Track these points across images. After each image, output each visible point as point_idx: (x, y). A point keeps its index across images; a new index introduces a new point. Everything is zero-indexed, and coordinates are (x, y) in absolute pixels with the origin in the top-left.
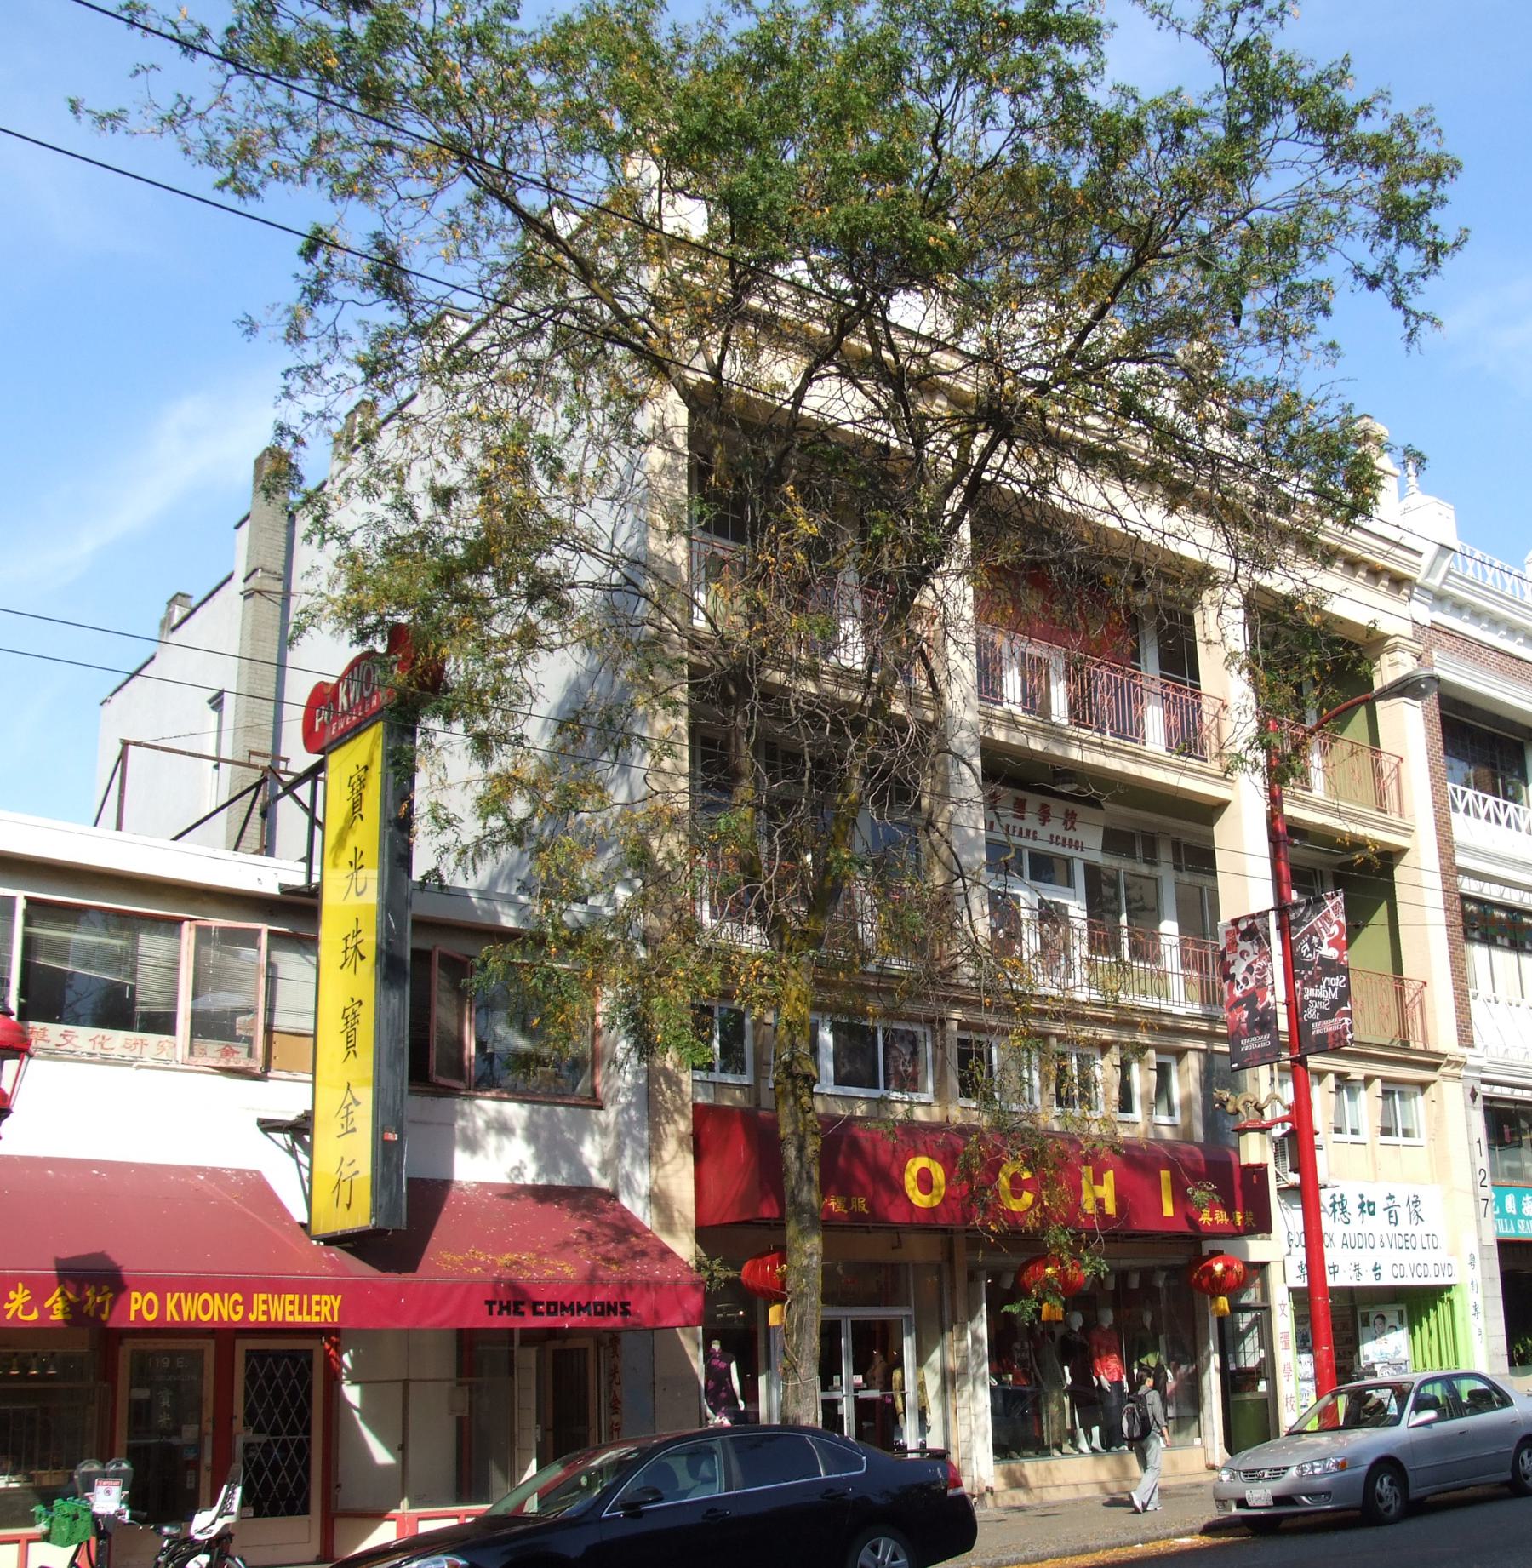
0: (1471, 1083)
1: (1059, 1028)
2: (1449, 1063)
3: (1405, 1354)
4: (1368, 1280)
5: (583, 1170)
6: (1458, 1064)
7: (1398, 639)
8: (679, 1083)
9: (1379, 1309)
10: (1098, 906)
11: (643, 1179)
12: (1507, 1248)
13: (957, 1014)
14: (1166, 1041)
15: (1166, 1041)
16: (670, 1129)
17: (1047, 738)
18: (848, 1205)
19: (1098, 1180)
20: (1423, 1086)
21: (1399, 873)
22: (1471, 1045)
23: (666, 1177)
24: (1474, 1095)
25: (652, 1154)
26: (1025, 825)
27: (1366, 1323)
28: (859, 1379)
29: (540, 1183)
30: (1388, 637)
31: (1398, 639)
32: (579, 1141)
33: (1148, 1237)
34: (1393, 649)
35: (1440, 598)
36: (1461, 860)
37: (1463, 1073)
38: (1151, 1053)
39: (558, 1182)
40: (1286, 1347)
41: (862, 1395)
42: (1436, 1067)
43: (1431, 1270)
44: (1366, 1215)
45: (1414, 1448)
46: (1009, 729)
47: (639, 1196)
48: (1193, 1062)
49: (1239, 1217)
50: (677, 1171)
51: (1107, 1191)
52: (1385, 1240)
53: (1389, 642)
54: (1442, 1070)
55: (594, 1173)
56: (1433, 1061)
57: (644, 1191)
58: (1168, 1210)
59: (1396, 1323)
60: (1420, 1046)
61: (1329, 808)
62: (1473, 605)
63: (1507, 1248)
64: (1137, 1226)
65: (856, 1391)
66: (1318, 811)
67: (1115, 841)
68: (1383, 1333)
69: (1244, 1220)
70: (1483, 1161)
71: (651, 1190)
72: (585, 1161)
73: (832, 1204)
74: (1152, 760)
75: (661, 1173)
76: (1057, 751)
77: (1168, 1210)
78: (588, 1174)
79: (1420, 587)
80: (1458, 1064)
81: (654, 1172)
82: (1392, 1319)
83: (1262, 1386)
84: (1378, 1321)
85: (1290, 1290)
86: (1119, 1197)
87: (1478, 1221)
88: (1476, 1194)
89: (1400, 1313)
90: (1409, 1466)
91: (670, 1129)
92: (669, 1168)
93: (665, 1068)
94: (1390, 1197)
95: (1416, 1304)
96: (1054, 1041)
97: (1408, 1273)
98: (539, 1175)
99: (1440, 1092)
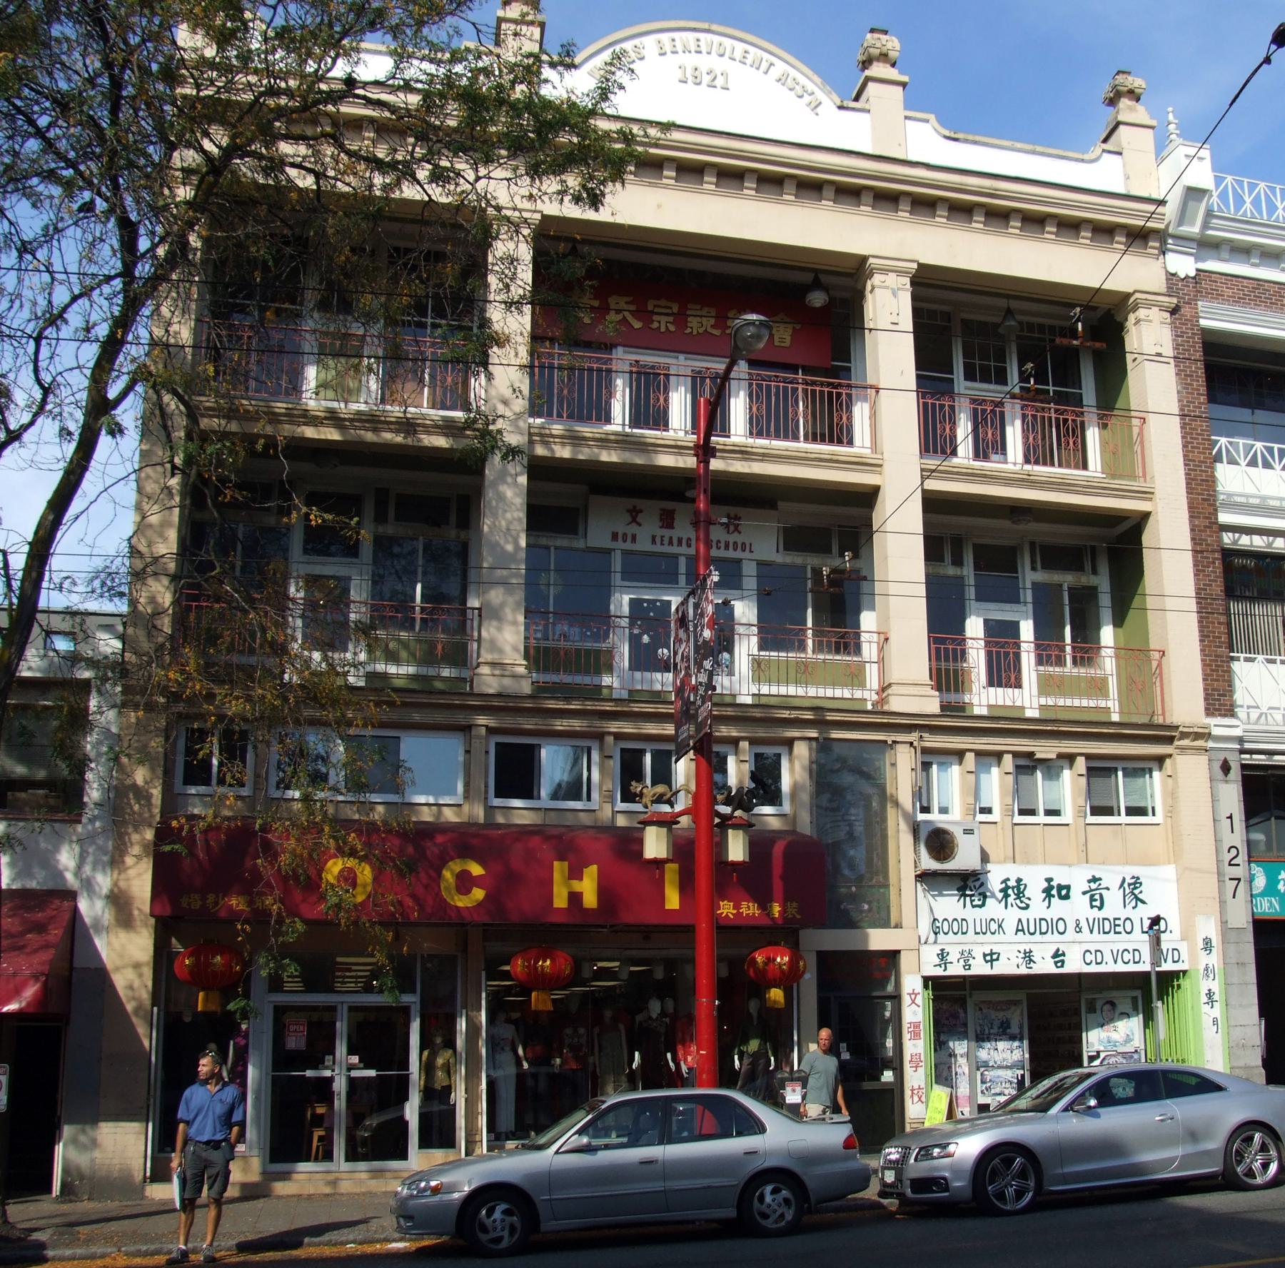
0: (1222, 756)
1: (614, 726)
2: (1184, 735)
3: (1138, 1042)
4: (980, 968)
5: (59, 875)
6: (1198, 736)
7: (1137, 295)
8: (149, 797)
9: (1114, 994)
10: (766, 601)
11: (104, 881)
12: (1264, 929)
13: (482, 720)
14: (761, 733)
15: (761, 733)
16: (135, 837)
17: (623, 449)
18: (250, 903)
19: (575, 874)
20: (1160, 760)
21: (1147, 539)
22: (1230, 711)
23: (128, 880)
24: (1226, 768)
25: (116, 861)
26: (675, 534)
27: (1092, 1009)
28: (355, 1059)
29: (14, 887)
30: (1128, 295)
31: (1137, 295)
32: (57, 849)
33: (647, 932)
34: (1135, 308)
35: (1207, 246)
36: (1224, 518)
37: (1211, 744)
38: (744, 745)
39: (33, 884)
40: (916, 1035)
41: (354, 1074)
42: (1170, 740)
43: (1108, 957)
44: (1055, 900)
45: (552, 1179)
46: (574, 445)
47: (100, 897)
48: (801, 749)
49: (776, 909)
50: (140, 875)
51: (588, 887)
52: (1083, 924)
53: (1132, 300)
54: (1176, 743)
55: (69, 876)
56: (1166, 735)
57: (105, 891)
58: (673, 900)
59: (1129, 1010)
60: (1161, 721)
61: (1023, 480)
62: (1231, 241)
63: (1264, 929)
64: (628, 918)
65: (349, 1070)
66: (1042, 489)
67: (795, 539)
68: (1112, 1020)
69: (782, 913)
70: (1237, 837)
71: (112, 891)
72: (61, 867)
73: (234, 902)
74: (764, 455)
75: (123, 876)
76: (639, 460)
77: (673, 900)
78: (64, 878)
79: (1173, 237)
80: (1198, 736)
81: (115, 876)
82: (1125, 1005)
83: (888, 1076)
84: (1107, 1007)
85: (926, 980)
86: (602, 891)
87: (1222, 903)
88: (1220, 873)
89: (1134, 1000)
90: (541, 1198)
91: (135, 837)
92: (131, 872)
93: (135, 785)
94: (1094, 880)
95: (1146, 991)
96: (610, 739)
97: (1108, 957)
98: (13, 880)
99: (1174, 765)
